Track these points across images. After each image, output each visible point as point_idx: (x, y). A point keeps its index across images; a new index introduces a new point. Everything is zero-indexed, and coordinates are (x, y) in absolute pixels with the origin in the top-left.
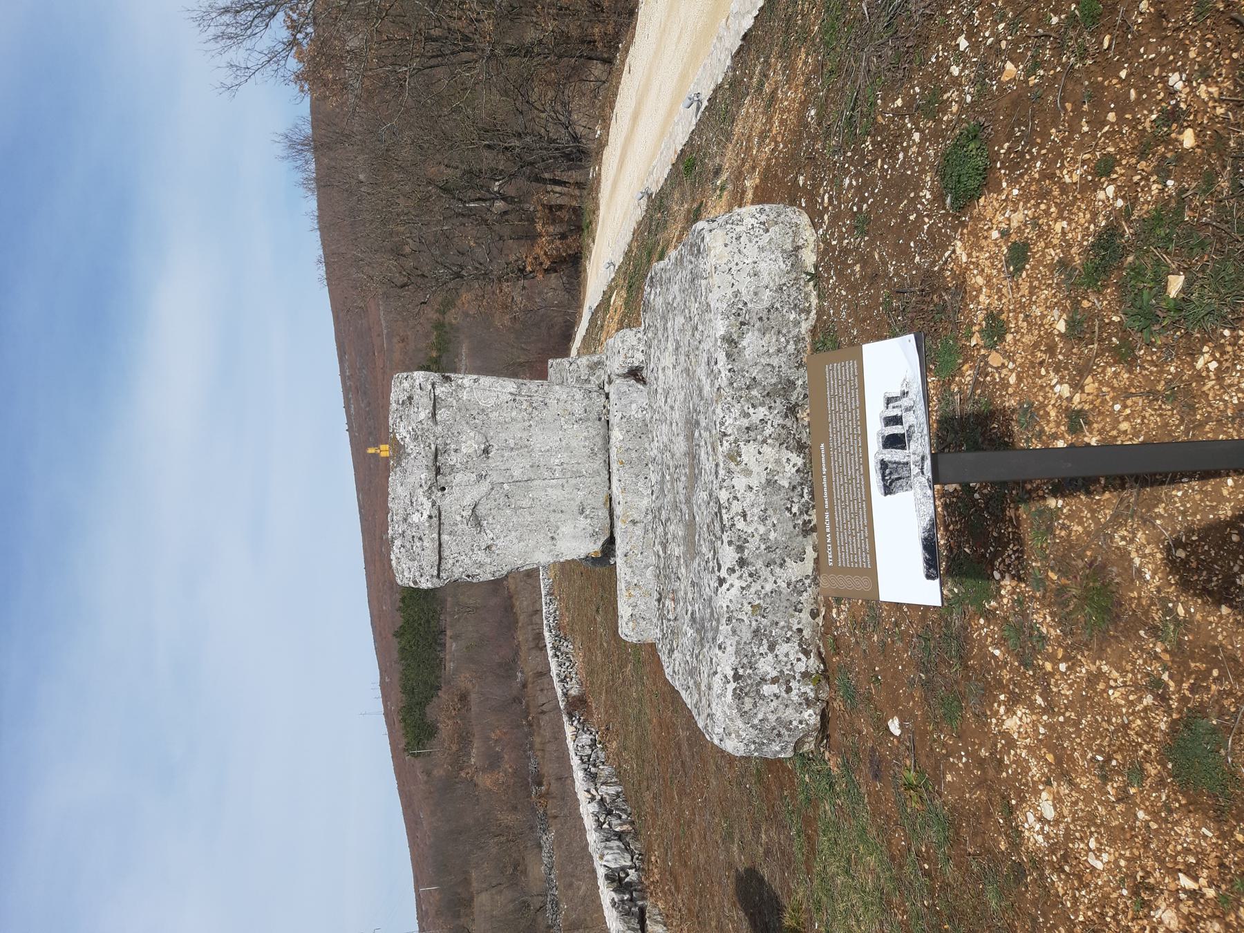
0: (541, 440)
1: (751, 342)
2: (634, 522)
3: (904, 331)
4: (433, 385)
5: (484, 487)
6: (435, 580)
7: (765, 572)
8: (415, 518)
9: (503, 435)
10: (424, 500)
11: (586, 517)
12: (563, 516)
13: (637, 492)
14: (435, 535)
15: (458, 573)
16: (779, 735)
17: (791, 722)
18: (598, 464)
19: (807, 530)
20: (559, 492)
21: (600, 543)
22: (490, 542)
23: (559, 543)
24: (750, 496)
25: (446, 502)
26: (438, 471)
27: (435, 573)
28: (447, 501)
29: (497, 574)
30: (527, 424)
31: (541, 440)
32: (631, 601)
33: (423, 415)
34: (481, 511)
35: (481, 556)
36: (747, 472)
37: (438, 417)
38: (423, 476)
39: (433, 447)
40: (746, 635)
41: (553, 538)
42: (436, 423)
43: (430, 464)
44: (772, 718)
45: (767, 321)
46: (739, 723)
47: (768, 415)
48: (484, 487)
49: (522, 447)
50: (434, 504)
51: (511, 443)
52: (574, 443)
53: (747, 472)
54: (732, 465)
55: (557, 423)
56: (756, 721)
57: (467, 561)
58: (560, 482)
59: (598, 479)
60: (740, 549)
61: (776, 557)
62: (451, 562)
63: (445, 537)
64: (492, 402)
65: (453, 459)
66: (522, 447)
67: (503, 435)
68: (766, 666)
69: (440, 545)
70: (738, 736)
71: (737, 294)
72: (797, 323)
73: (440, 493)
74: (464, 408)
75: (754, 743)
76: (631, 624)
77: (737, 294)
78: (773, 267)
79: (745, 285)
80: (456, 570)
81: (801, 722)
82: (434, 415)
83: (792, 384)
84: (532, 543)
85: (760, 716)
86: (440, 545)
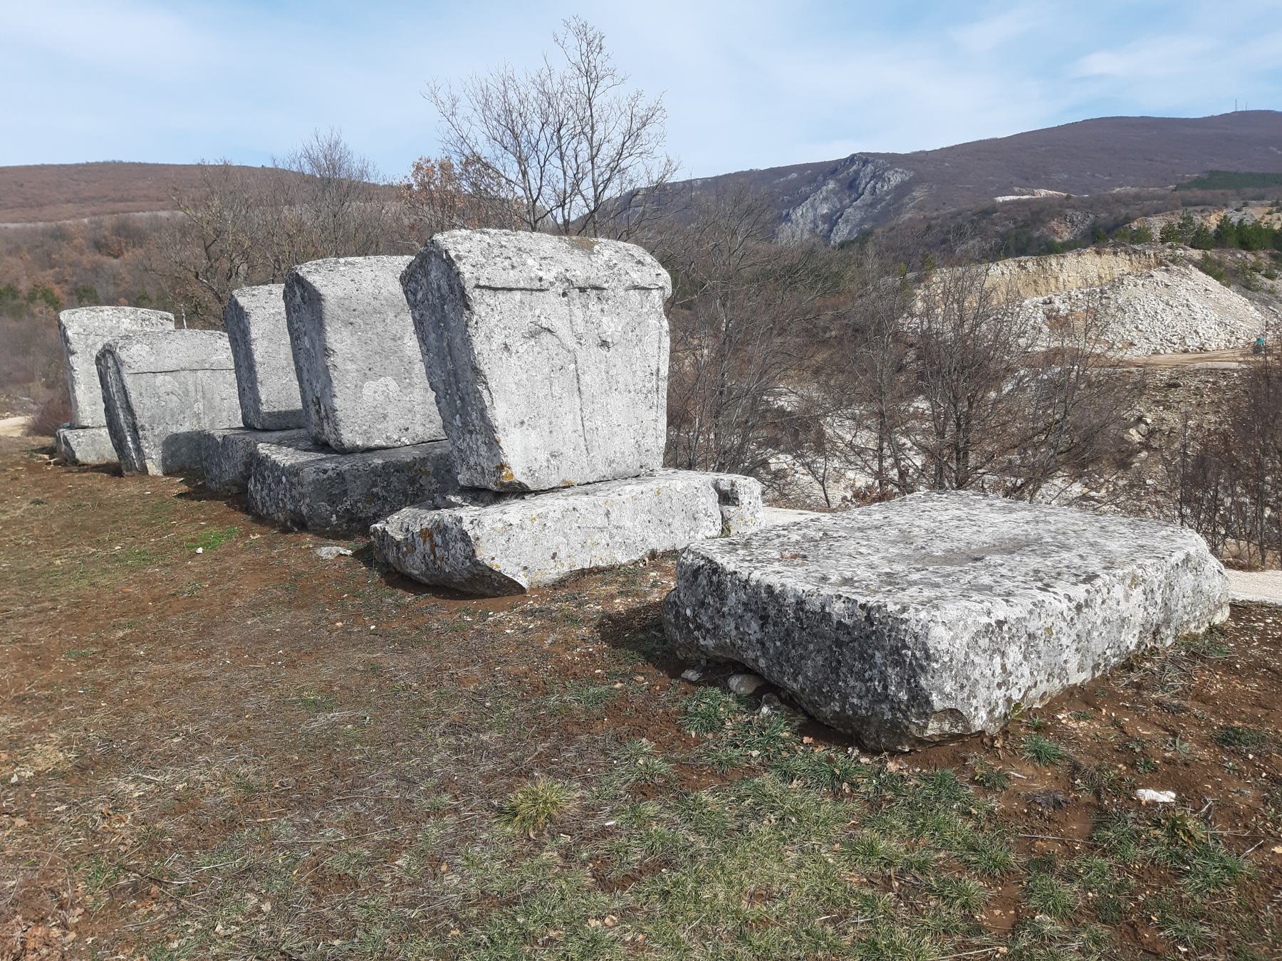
2: (608, 514)
3: (1028, 726)
4: (662, 288)
5: (571, 342)
6: (474, 282)
9: (619, 364)
10: (553, 273)
11: (548, 461)
12: (546, 434)
13: (635, 513)
14: (522, 285)
15: (479, 309)
16: (962, 687)
17: (975, 697)
18: (603, 470)
21: (523, 480)
22: (513, 349)
23: (517, 431)
25: (552, 297)
26: (582, 290)
27: (482, 283)
29: (481, 358)
30: (632, 388)
32: (528, 522)
34: (545, 338)
35: (498, 339)
37: (632, 292)
38: (578, 273)
39: (606, 285)
41: (522, 423)
42: (627, 290)
43: (591, 282)
44: (976, 674)
46: (967, 637)
48: (571, 342)
50: (552, 284)
52: (617, 440)
54: (1128, 581)
55: (634, 421)
56: (972, 656)
57: (493, 322)
58: (580, 427)
59: (587, 471)
62: (492, 302)
63: (518, 295)
65: (595, 307)
67: (619, 364)
68: (1014, 653)
69: (511, 290)
70: (954, 639)
73: (561, 291)
75: (951, 660)
76: (500, 525)
80: (482, 305)
81: (976, 708)
82: (635, 288)
84: (515, 399)
85: (977, 660)
86: (511, 290)
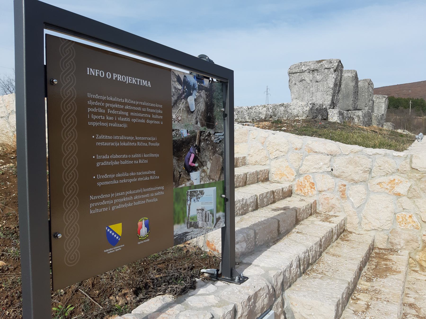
0: (319, 94)
1: (282, 108)
5: (309, 82)
7: (247, 113)
8: (303, 67)
19: (253, 120)
20: (306, 99)
24: (258, 110)
25: (306, 73)
26: (313, 71)
28: (306, 74)
31: (319, 94)
33: (326, 66)
34: (304, 82)
36: (262, 109)
40: (238, 110)
45: (286, 111)
47: (270, 112)
48: (309, 82)
49: (318, 90)
51: (318, 87)
53: (262, 109)
60: (251, 108)
61: (249, 114)
63: (298, 74)
64: (329, 82)
66: (318, 90)
71: (291, 106)
72: (285, 117)
74: (328, 75)
77: (291, 106)
78: (295, 112)
79: (292, 107)
82: (326, 69)
83: (275, 116)
84: (296, 94)
